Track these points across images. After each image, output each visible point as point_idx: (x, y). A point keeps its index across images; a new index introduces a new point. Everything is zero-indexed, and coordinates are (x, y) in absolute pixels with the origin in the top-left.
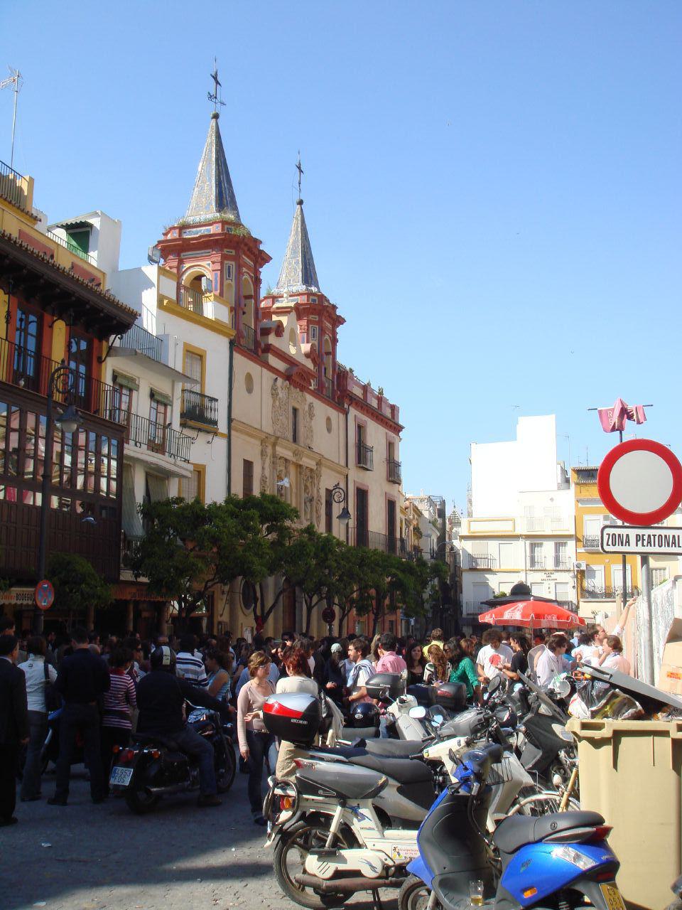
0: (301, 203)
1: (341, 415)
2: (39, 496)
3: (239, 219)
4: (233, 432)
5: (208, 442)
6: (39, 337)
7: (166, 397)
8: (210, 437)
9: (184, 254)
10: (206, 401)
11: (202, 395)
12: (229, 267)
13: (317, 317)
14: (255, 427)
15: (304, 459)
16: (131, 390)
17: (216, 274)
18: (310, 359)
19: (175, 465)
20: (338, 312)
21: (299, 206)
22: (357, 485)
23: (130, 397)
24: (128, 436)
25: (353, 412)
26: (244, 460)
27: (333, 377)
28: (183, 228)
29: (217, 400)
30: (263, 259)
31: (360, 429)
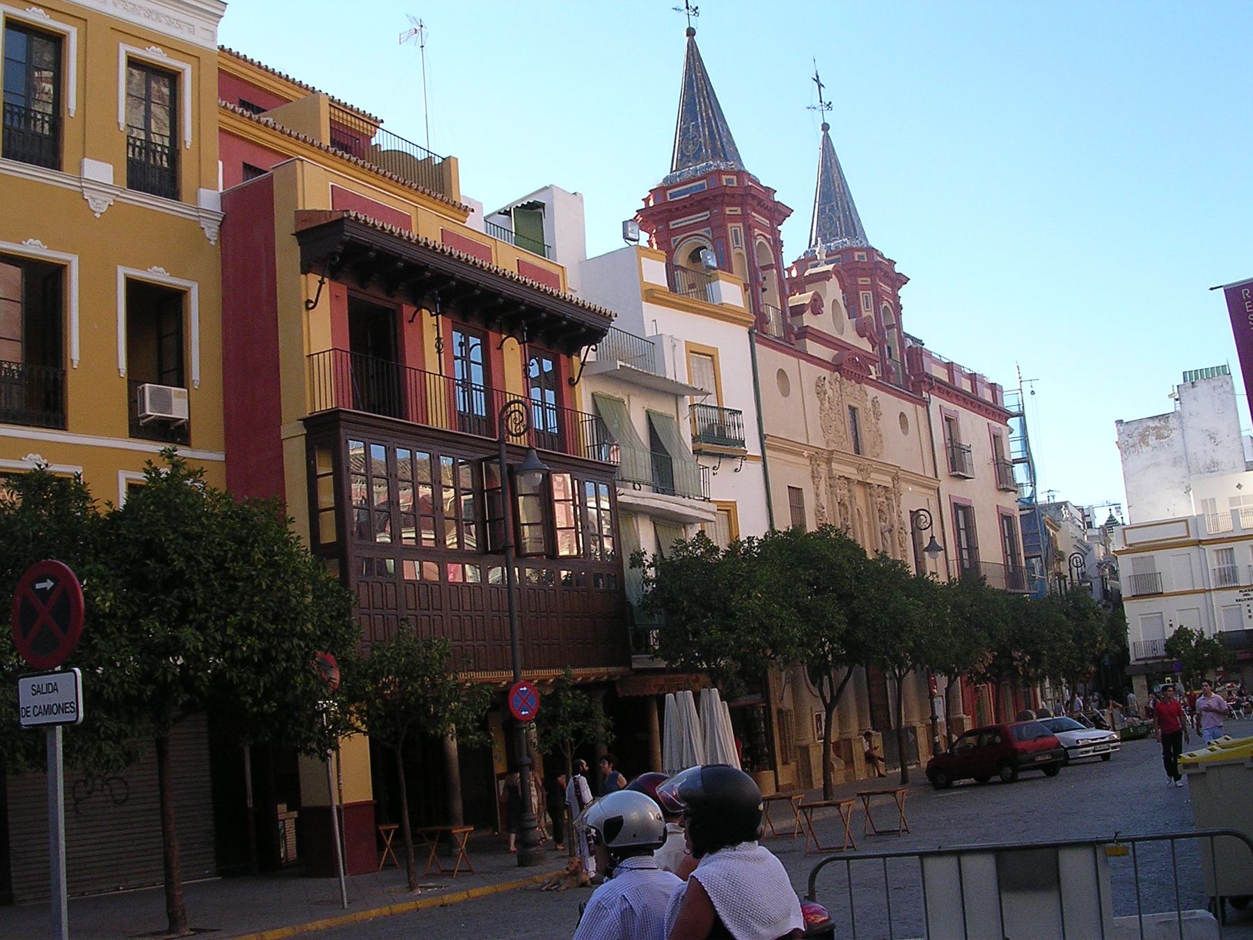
1: (923, 406)
4: (767, 452)
8: (737, 463)
11: (721, 409)
15: (873, 475)
20: (898, 269)
25: (936, 402)
30: (780, 213)
31: (950, 421)
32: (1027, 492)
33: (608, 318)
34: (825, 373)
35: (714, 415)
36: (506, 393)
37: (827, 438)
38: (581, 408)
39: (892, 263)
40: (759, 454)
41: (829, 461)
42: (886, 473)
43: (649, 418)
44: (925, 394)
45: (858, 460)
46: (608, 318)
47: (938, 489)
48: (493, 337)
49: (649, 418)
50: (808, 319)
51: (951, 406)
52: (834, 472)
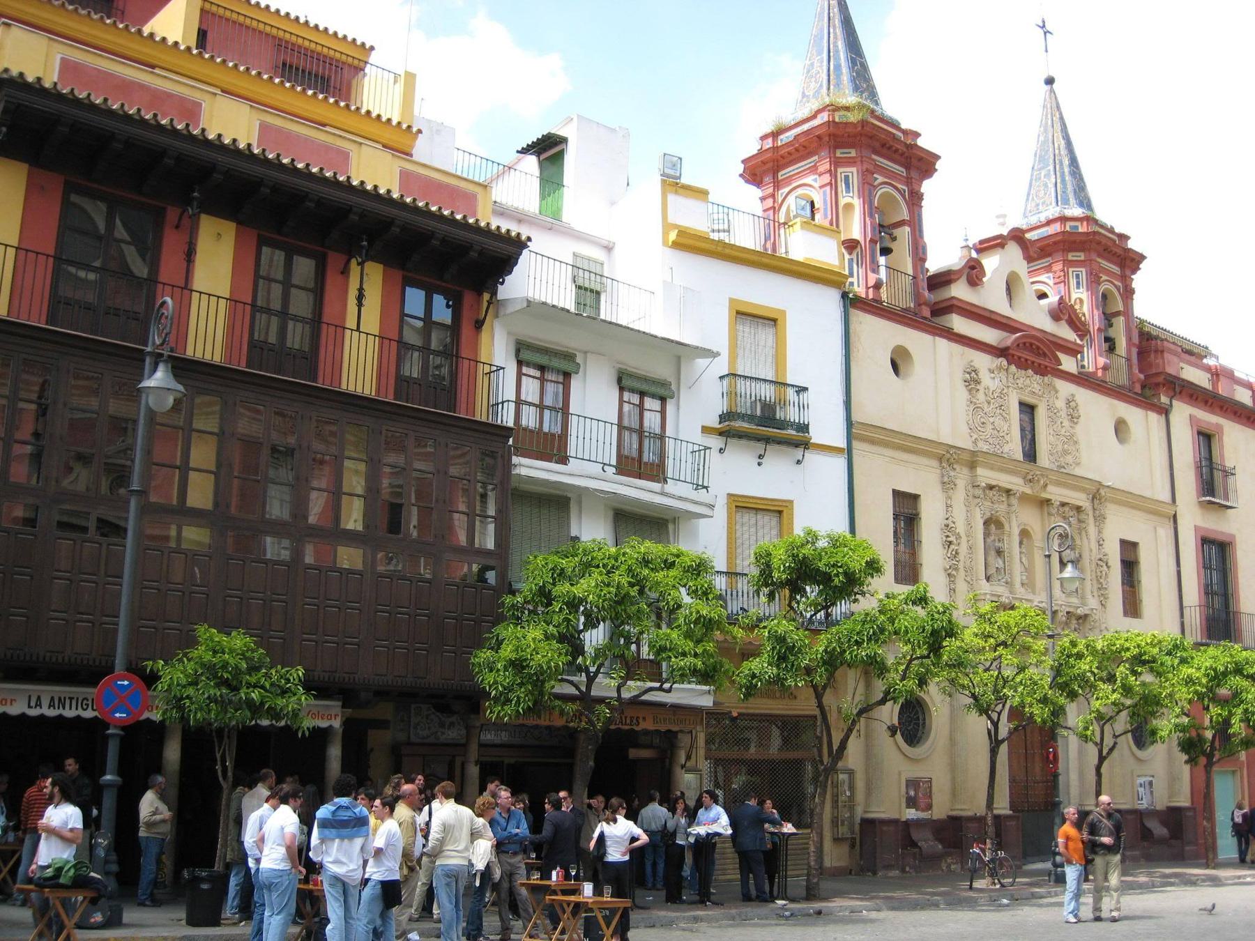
0: (1050, 81)
1: (1153, 417)
2: (309, 559)
3: (873, 95)
4: (855, 444)
5: (799, 462)
6: (318, 292)
7: (664, 384)
8: (799, 453)
9: (783, 172)
10: (791, 394)
11: (781, 384)
12: (847, 178)
13: (904, 170)
14: (1161, 499)
15: (1050, 488)
16: (663, 400)
17: (825, 193)
18: (1063, 323)
19: (663, 494)
20: (1131, 244)
21: (1048, 87)
22: (1203, 533)
23: (663, 413)
24: (664, 473)
25: (1182, 413)
26: (894, 491)
27: (1129, 351)
28: (775, 134)
29: (805, 389)
30: (1133, 260)
31: (1206, 438)
32: (1068, 364)
33: (367, 50)
34: (983, 361)
35: (767, 392)
36: (344, 328)
37: (975, 436)
38: (491, 354)
39: (1123, 237)
40: (842, 443)
41: (972, 466)
42: (1083, 490)
43: (1150, 917)
44: (1164, 399)
45: (1028, 466)
46: (367, 50)
47: (1175, 516)
48: (335, 260)
49: (1150, 917)
50: (959, 291)
51: (1210, 419)
52: (979, 479)
